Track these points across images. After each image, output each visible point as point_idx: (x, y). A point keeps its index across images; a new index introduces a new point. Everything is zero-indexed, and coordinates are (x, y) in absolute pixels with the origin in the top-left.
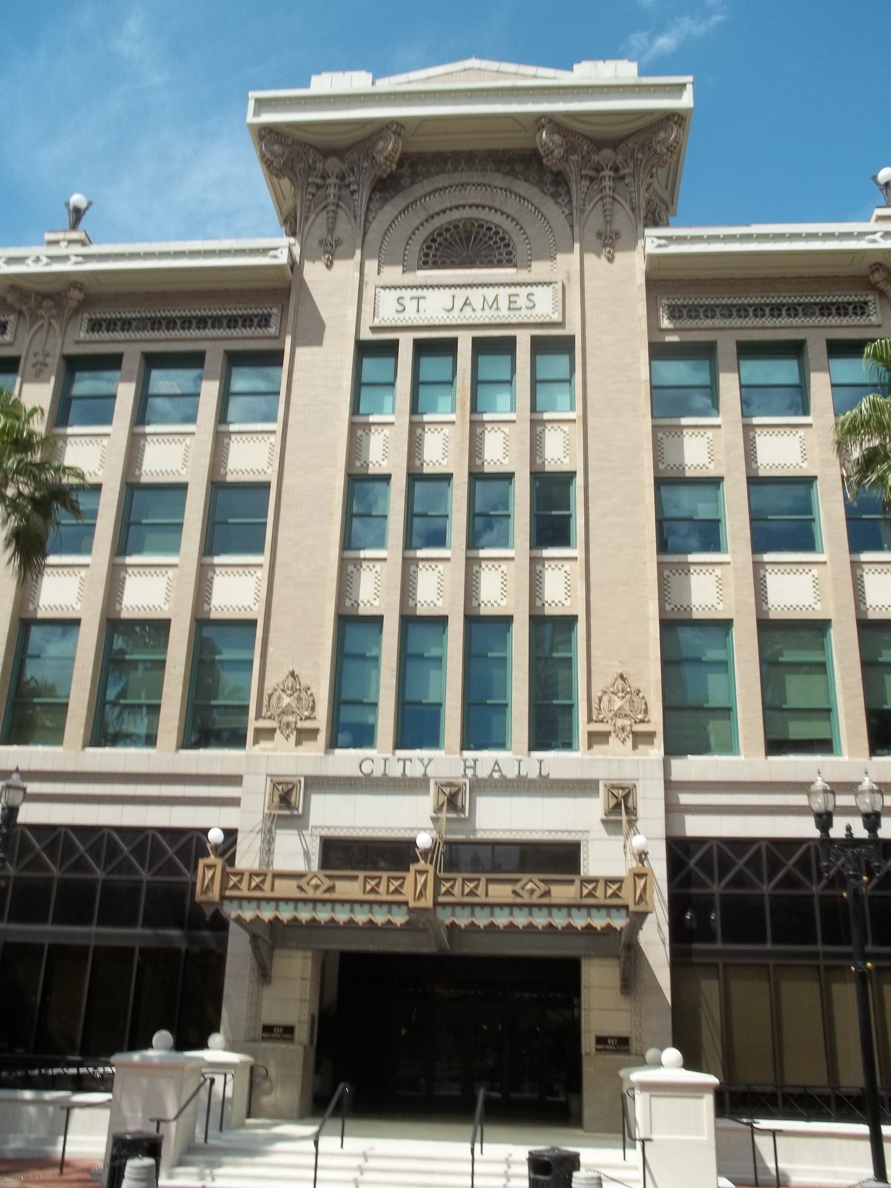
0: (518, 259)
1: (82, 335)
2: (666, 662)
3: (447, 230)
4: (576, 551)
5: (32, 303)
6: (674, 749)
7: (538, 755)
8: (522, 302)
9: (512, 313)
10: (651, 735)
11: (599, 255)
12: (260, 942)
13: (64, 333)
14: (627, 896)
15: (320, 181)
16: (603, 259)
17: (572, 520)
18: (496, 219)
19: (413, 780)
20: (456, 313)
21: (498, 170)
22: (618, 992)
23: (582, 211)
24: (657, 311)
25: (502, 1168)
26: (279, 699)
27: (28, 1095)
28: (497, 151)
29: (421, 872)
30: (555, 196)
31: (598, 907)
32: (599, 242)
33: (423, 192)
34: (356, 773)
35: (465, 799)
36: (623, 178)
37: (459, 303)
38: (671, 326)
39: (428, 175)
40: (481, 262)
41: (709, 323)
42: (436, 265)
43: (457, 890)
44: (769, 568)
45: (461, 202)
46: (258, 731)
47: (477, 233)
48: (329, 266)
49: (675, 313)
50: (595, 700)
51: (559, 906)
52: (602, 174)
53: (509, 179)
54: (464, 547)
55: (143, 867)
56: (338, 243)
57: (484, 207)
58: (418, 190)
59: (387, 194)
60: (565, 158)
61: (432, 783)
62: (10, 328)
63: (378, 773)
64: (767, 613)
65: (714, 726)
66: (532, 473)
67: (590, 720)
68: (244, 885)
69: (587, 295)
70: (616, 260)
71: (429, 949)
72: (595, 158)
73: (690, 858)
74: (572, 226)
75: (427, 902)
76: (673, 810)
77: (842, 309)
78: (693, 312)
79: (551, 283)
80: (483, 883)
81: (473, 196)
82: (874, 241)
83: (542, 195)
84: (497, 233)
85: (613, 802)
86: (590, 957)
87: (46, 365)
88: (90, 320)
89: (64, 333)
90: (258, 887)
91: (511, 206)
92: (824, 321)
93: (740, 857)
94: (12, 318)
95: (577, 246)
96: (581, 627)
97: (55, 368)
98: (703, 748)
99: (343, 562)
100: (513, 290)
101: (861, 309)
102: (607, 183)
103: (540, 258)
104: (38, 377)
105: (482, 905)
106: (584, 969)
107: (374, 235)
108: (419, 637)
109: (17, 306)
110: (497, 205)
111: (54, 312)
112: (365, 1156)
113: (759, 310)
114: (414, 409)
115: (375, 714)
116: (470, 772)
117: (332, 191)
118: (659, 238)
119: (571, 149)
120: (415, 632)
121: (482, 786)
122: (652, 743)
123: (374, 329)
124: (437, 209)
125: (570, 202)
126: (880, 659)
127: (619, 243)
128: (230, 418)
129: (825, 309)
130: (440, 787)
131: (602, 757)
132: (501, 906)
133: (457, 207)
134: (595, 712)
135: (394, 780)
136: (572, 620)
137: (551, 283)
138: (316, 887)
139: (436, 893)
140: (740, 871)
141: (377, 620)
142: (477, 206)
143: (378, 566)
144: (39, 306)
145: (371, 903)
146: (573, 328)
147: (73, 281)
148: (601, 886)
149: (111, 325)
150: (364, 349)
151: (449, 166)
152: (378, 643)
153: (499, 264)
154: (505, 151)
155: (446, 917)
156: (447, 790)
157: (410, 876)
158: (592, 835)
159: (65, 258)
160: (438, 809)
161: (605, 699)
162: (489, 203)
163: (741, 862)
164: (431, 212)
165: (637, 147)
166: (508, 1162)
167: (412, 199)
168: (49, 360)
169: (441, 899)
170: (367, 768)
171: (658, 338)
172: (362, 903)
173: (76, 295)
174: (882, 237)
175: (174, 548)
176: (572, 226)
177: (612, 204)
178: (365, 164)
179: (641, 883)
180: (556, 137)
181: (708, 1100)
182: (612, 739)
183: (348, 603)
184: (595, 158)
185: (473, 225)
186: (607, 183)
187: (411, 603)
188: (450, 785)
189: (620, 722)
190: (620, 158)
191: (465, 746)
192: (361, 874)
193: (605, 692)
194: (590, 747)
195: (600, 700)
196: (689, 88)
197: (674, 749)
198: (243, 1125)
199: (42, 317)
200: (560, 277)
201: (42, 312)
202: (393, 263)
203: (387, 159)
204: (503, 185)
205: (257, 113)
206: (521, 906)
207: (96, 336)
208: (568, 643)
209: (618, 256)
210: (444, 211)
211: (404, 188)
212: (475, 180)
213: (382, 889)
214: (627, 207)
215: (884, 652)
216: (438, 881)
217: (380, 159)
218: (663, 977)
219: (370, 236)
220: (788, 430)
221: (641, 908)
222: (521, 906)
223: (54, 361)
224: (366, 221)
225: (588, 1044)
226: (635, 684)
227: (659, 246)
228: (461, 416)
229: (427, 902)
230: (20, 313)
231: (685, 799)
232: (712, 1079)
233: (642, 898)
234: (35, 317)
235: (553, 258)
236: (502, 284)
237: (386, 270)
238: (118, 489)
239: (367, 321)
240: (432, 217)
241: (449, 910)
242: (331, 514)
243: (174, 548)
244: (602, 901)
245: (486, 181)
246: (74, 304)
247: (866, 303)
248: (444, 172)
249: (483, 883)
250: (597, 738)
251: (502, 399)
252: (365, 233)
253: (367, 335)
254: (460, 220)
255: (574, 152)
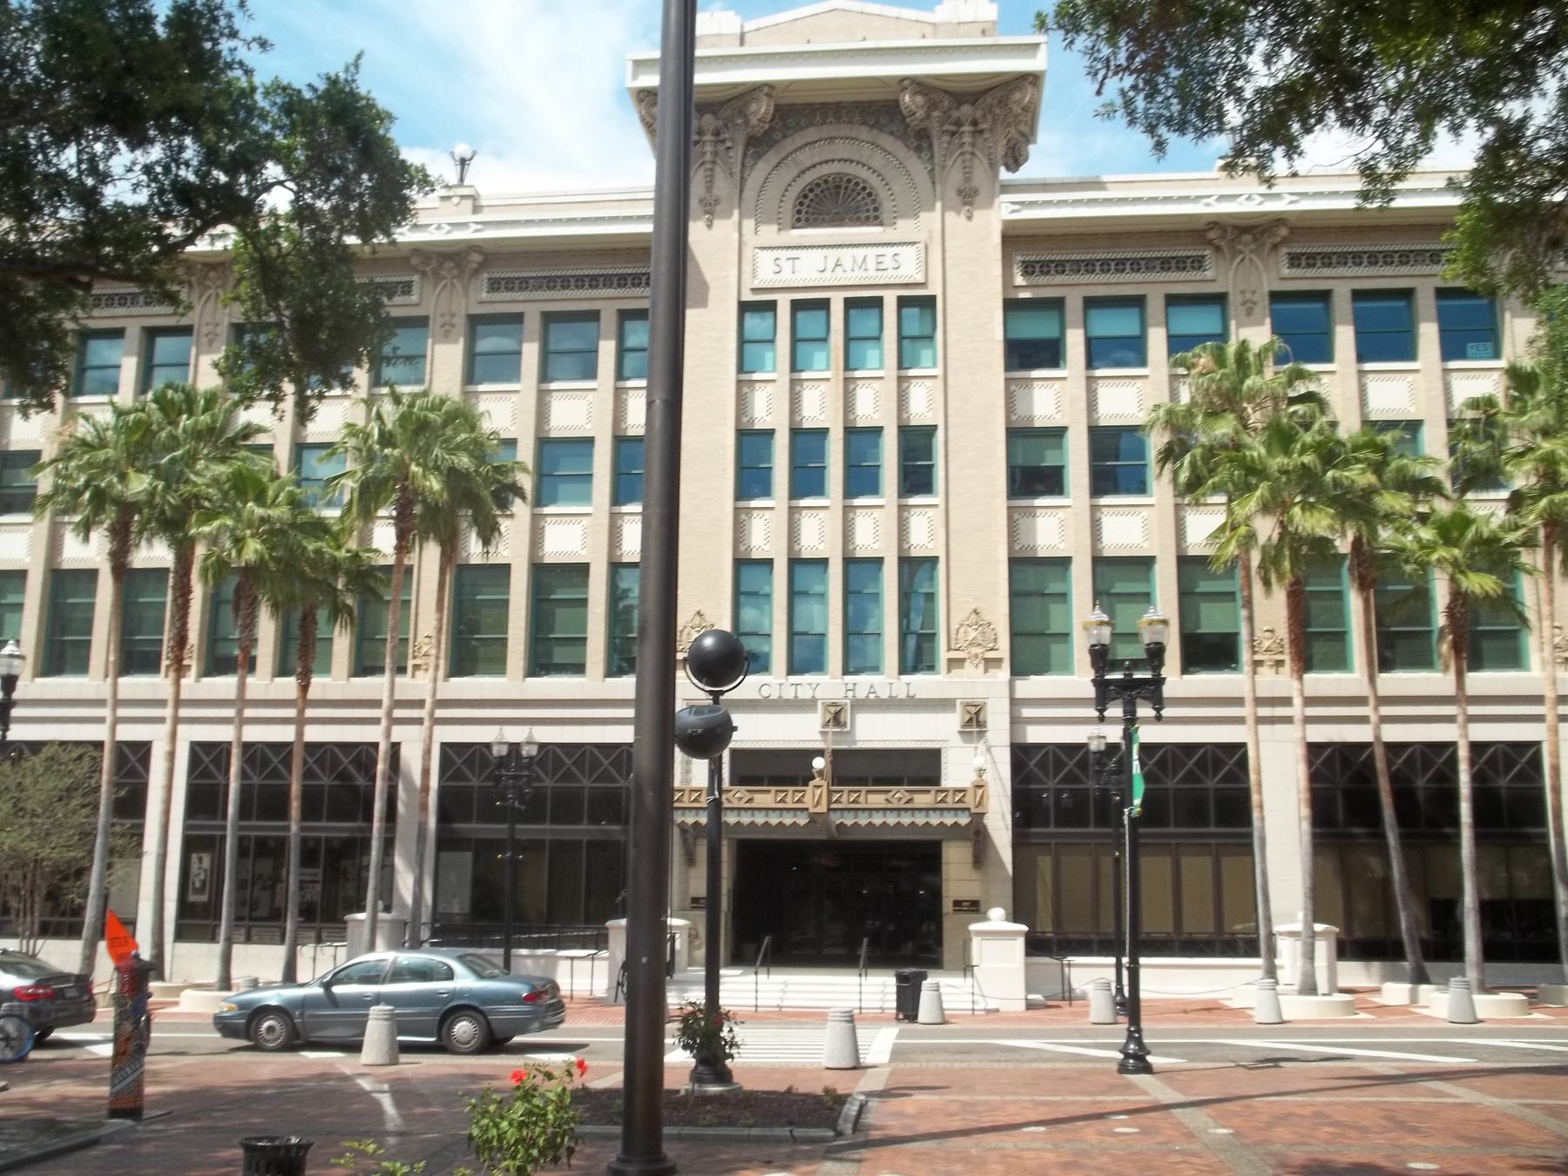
0: (885, 216)
1: (484, 295)
2: (1013, 594)
3: (818, 185)
4: (936, 499)
5: (434, 264)
6: (1018, 670)
7: (906, 678)
8: (888, 262)
9: (881, 273)
10: (999, 661)
11: (958, 213)
12: (688, 836)
13: (466, 293)
14: (970, 802)
15: (953, 128)
16: (963, 218)
17: (934, 470)
18: (864, 174)
19: (803, 701)
20: (827, 274)
21: (864, 123)
22: (970, 866)
23: (943, 167)
24: (1011, 268)
25: (881, 988)
26: (689, 634)
27: (524, 952)
28: (864, 102)
29: (819, 787)
30: (918, 149)
31: (949, 809)
32: (958, 200)
33: (794, 147)
34: (757, 696)
35: (847, 716)
36: (981, 132)
37: (831, 265)
38: (1024, 283)
39: (799, 128)
40: (851, 220)
41: (1059, 279)
42: (809, 223)
43: (844, 799)
44: (1105, 510)
45: (830, 157)
46: (950, 661)
47: (846, 188)
48: (710, 226)
49: (1028, 269)
50: (953, 632)
51: (920, 810)
52: (963, 129)
53: (875, 131)
54: (841, 497)
55: (584, 776)
56: (717, 201)
57: (852, 161)
58: (789, 144)
59: (759, 149)
60: (928, 117)
61: (819, 703)
62: (416, 288)
63: (774, 696)
64: (1101, 550)
65: (1056, 649)
66: (900, 428)
67: (949, 649)
68: (686, 798)
69: (948, 255)
70: (975, 218)
71: (823, 836)
72: (955, 114)
73: (1031, 760)
74: (934, 183)
75: (823, 808)
76: (1016, 721)
77: (1181, 264)
78: (1045, 268)
79: (915, 243)
80: (863, 793)
81: (841, 149)
82: (1208, 205)
83: (906, 149)
84: (864, 188)
85: (967, 717)
86: (949, 840)
87: (453, 326)
88: (490, 279)
89: (466, 293)
90: (696, 800)
91: (878, 160)
92: (1164, 276)
93: (1071, 759)
94: (416, 278)
95: (938, 205)
96: (941, 566)
97: (462, 329)
98: (1042, 668)
99: (737, 511)
100: (880, 250)
101: (1198, 263)
102: (967, 139)
103: (905, 216)
104: (446, 337)
105: (864, 810)
106: (944, 850)
107: (749, 194)
108: (805, 576)
109: (421, 268)
110: (863, 160)
111: (455, 272)
112: (785, 983)
113: (1105, 266)
114: (794, 368)
115: (770, 643)
116: (850, 694)
117: (708, 148)
118: (1013, 203)
119: (932, 106)
120: (800, 571)
121: (859, 705)
122: (999, 667)
123: (755, 290)
124: (808, 165)
125: (932, 157)
126: (1197, 590)
127: (978, 200)
128: (627, 373)
129: (1165, 264)
130: (827, 706)
131: (958, 680)
132: (878, 810)
133: (826, 162)
134: (953, 642)
135: (787, 701)
136: (934, 560)
137: (915, 243)
138: (740, 799)
139: (829, 802)
140: (1070, 770)
141: (768, 563)
142: (846, 161)
143: (767, 514)
144: (441, 265)
145: (781, 809)
146: (934, 289)
147: (472, 247)
148: (951, 793)
149: (510, 285)
150: (745, 308)
151: (818, 118)
152: (770, 582)
153: (866, 221)
154: (871, 103)
155: (837, 819)
156: (833, 710)
157: (809, 789)
158: (950, 744)
159: (465, 225)
160: (826, 724)
161: (962, 630)
162: (856, 158)
163: (1072, 763)
164: (803, 168)
165: (995, 101)
166: (884, 985)
167: (783, 155)
168: (219, 330)
169: (833, 806)
170: (765, 692)
171: (1012, 295)
172: (774, 809)
173: (1284, 232)
174: (1217, 200)
175: (586, 498)
176: (934, 183)
177: (971, 160)
178: (739, 121)
179: (980, 792)
180: (919, 99)
181: (1020, 944)
182: (967, 664)
183: (742, 548)
184: (955, 114)
185: (841, 179)
186: (967, 139)
187: (797, 548)
188: (834, 705)
189: (975, 650)
190: (979, 114)
191: (846, 672)
192: (773, 789)
193: (962, 625)
194: (949, 671)
195: (958, 630)
196: (1043, 48)
197: (1018, 670)
198: (686, 971)
199: (1240, 252)
200: (921, 236)
201: (444, 273)
202: (769, 222)
203: (760, 120)
204: (868, 139)
205: (635, 77)
206: (892, 810)
207: (497, 296)
208: (932, 578)
209: (977, 214)
210: (814, 166)
211: (776, 142)
212: (842, 134)
213: (789, 799)
214: (985, 161)
215: (1201, 583)
216: (830, 793)
217: (754, 121)
218: (1006, 853)
219: (748, 194)
220: (1127, 381)
221: (979, 810)
222: (892, 810)
223: (461, 322)
224: (742, 178)
225: (947, 906)
226: (987, 617)
227: (1013, 211)
228: (836, 373)
229: (823, 808)
230: (424, 274)
231: (1027, 712)
232: (1024, 928)
233: (980, 804)
234: (438, 277)
235: (916, 216)
236: (870, 245)
237: (763, 228)
238: (532, 446)
239: (748, 283)
240: (803, 172)
241: (839, 813)
242: (725, 469)
243: (586, 498)
244: (951, 805)
245: (853, 135)
246: (474, 266)
247: (1203, 257)
248: (813, 125)
249: (863, 793)
250: (955, 663)
251: (872, 354)
252: (741, 191)
253: (748, 297)
254: (829, 175)
255: (936, 108)
